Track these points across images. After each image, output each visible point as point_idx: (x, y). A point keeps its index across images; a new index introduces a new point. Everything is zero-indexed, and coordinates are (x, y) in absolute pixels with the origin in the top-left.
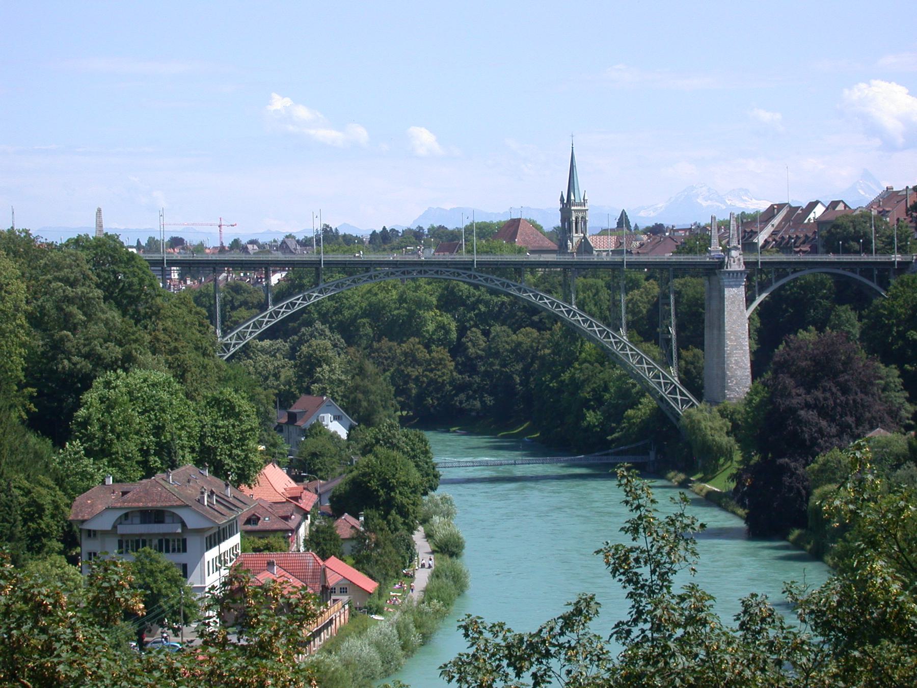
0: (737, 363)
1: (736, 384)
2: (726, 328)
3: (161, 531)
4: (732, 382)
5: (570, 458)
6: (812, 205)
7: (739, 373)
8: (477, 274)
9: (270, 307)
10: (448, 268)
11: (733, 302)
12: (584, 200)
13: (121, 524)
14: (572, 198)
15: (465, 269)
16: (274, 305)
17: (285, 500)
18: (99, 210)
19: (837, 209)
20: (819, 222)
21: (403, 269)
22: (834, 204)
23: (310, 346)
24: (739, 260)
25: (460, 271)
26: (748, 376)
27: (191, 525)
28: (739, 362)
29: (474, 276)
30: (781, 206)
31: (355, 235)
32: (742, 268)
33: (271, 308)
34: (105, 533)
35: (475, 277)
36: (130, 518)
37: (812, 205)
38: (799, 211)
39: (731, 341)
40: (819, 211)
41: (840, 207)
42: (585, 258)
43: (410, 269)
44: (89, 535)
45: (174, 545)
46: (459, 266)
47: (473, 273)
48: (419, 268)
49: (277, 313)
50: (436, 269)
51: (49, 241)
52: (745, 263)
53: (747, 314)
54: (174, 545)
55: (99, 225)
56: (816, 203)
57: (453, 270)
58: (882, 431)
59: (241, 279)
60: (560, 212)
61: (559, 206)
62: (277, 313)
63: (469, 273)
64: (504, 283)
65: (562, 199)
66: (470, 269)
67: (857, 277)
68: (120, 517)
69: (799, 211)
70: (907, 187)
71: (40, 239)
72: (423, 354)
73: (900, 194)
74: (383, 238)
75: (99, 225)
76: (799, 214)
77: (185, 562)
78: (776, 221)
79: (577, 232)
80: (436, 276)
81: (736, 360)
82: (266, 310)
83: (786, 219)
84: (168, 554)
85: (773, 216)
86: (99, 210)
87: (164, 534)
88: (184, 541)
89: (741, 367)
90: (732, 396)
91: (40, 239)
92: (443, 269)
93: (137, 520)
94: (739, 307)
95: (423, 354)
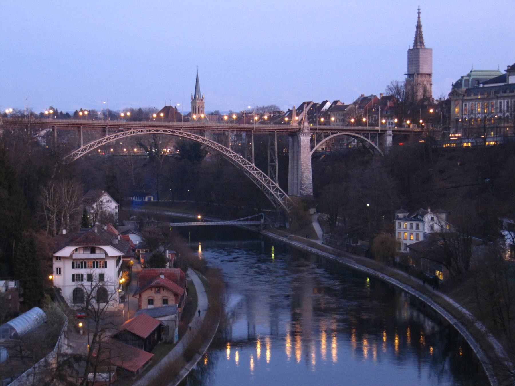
1: (306, 187)
3: (95, 257)
4: (304, 186)
6: (324, 103)
7: (307, 182)
8: (134, 130)
10: (169, 129)
11: (304, 148)
12: (203, 97)
13: (73, 254)
24: (308, 128)
25: (175, 131)
26: (311, 183)
27: (110, 254)
28: (307, 177)
29: (182, 133)
30: (308, 103)
33: (82, 147)
34: (65, 258)
35: (182, 134)
36: (78, 250)
37: (324, 103)
39: (303, 166)
40: (328, 105)
41: (338, 104)
43: (151, 129)
44: (57, 259)
45: (100, 265)
46: (174, 128)
47: (181, 131)
48: (155, 129)
49: (85, 149)
53: (311, 153)
54: (100, 265)
56: (326, 102)
57: (171, 130)
62: (85, 149)
63: (179, 131)
64: (124, 133)
65: (192, 98)
66: (180, 130)
68: (73, 251)
73: (368, 98)
77: (73, 269)
81: (306, 176)
84: (97, 269)
87: (96, 259)
88: (106, 263)
89: (308, 179)
90: (304, 193)
92: (167, 130)
94: (308, 151)
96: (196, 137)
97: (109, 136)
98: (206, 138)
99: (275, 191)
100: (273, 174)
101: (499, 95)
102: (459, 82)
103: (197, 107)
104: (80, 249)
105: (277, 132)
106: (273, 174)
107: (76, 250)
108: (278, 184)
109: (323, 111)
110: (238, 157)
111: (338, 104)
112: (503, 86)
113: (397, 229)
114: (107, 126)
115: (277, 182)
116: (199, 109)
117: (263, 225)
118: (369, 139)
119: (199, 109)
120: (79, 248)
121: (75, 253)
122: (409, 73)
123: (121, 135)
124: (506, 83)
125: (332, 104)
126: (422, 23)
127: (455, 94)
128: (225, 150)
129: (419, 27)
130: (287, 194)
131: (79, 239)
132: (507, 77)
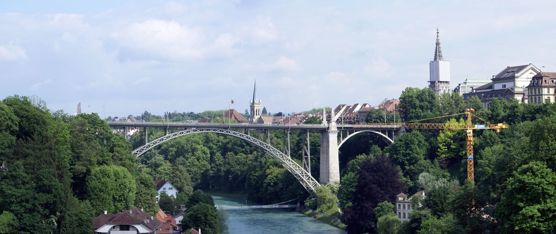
0: (334, 167)
2: (330, 154)
5: (254, 207)
6: (356, 105)
9: (147, 143)
13: (111, 230)
14: (255, 101)
15: (225, 129)
16: (148, 143)
17: (165, 222)
18: (80, 104)
19: (366, 107)
20: (360, 112)
21: (200, 129)
22: (365, 105)
23: (155, 159)
25: (223, 130)
30: (343, 106)
31: (90, 113)
32: (336, 129)
33: (147, 144)
36: (115, 228)
38: (351, 108)
40: (357, 109)
41: (367, 106)
42: (260, 125)
48: (207, 129)
50: (214, 129)
51: (71, 115)
52: (338, 128)
55: (79, 109)
56: (357, 105)
58: (403, 194)
59: (118, 132)
60: (250, 107)
61: (250, 105)
63: (227, 130)
66: (227, 129)
67: (380, 133)
68: (112, 228)
69: (351, 108)
70: (393, 99)
71: (68, 114)
72: (197, 163)
74: (170, 116)
75: (79, 109)
76: (350, 109)
78: (341, 111)
79: (257, 115)
80: (214, 132)
81: (334, 166)
82: (145, 144)
83: (346, 110)
85: (340, 109)
86: (80, 104)
91: (68, 114)
93: (118, 229)
95: (197, 163)
96: (240, 135)
97: (169, 135)
98: (249, 136)
99: (308, 179)
100: (306, 165)
101: (487, 99)
102: (457, 88)
103: (255, 110)
104: (117, 227)
105: (309, 130)
106: (306, 165)
107: (114, 227)
108: (310, 174)
109: (354, 113)
110: (276, 151)
111: (367, 106)
112: (490, 91)
113: (397, 210)
114: (167, 126)
115: (310, 172)
116: (256, 111)
117: (299, 208)
118: (386, 135)
119: (256, 111)
120: (116, 226)
121: (113, 229)
122: (432, 81)
123: (179, 134)
124: (492, 90)
125: (362, 107)
126: (440, 41)
127: (509, 93)
128: (265, 146)
129: (437, 44)
130: (319, 182)
131: (116, 218)
132: (493, 84)
